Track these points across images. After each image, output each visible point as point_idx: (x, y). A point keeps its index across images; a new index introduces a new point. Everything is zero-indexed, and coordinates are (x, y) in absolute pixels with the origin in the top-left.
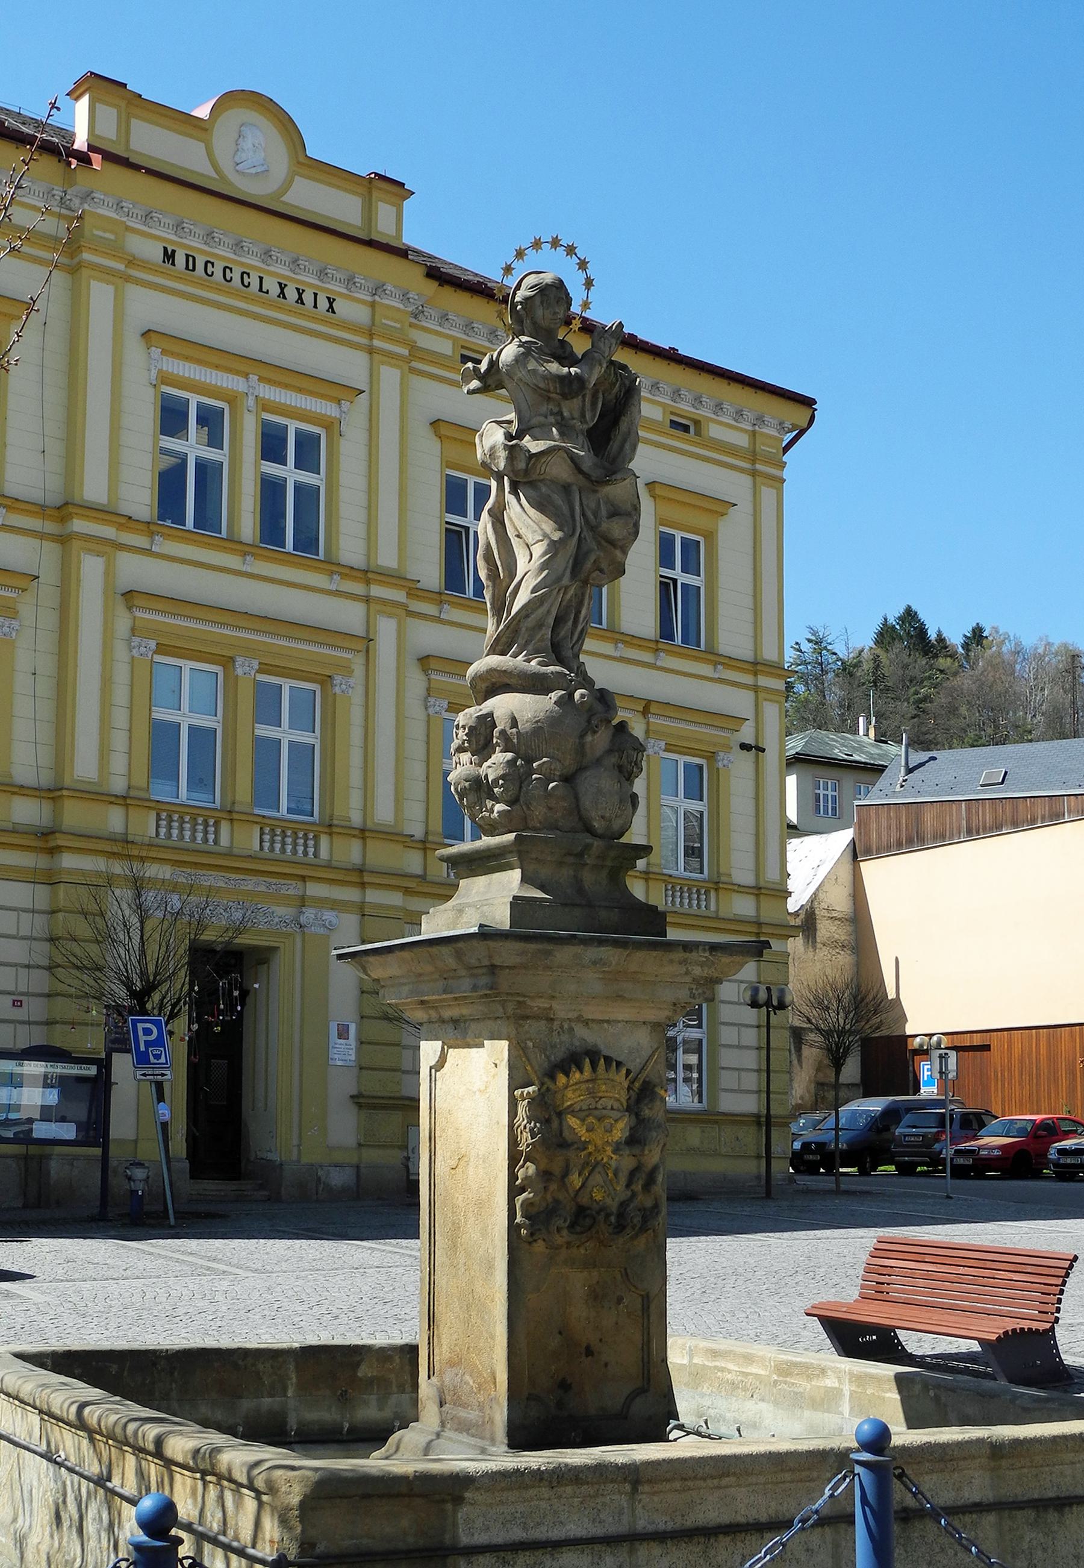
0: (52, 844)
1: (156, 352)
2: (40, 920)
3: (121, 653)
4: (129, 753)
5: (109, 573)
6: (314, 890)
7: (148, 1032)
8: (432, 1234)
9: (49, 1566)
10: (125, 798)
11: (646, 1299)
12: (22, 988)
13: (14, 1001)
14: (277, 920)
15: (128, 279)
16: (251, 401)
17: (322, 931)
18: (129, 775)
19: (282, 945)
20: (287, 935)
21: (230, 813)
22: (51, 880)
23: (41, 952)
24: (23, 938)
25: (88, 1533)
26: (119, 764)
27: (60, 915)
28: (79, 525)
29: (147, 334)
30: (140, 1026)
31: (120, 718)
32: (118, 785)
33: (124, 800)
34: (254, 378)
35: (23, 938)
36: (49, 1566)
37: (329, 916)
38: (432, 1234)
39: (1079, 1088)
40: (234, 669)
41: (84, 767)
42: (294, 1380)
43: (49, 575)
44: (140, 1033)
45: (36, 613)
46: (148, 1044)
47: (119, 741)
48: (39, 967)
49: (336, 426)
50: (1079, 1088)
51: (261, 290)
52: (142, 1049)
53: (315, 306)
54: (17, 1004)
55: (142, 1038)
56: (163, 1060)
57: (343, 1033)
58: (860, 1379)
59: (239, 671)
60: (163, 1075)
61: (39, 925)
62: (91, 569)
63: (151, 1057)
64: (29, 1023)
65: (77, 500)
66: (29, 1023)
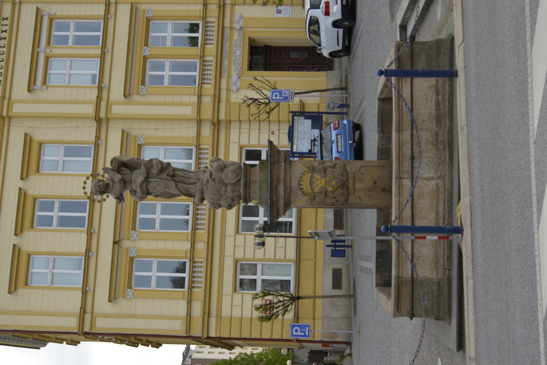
0: (217, 123)
1: (35, 87)
2: (243, 126)
4: (182, 95)
9: (350, 11)
12: (268, 131)
15: (10, 98)
17: (242, 20)
18: (190, 95)
19: (248, 36)
20: (244, 33)
21: (202, 57)
24: (250, 131)
26: (186, 99)
29: (29, 91)
31: (169, 99)
32: (194, 99)
33: (200, 97)
35: (250, 131)
36: (350, 11)
37: (237, 18)
39: (542, 339)
41: (189, 111)
42: (424, 59)
43: (126, 126)
45: (136, 129)
47: (177, 99)
49: (51, 17)
50: (542, 339)
51: (4, 47)
53: (2, 25)
57: (279, 12)
61: (245, 126)
62: (116, 110)
64: (279, 130)
65: (94, 115)
66: (279, 130)
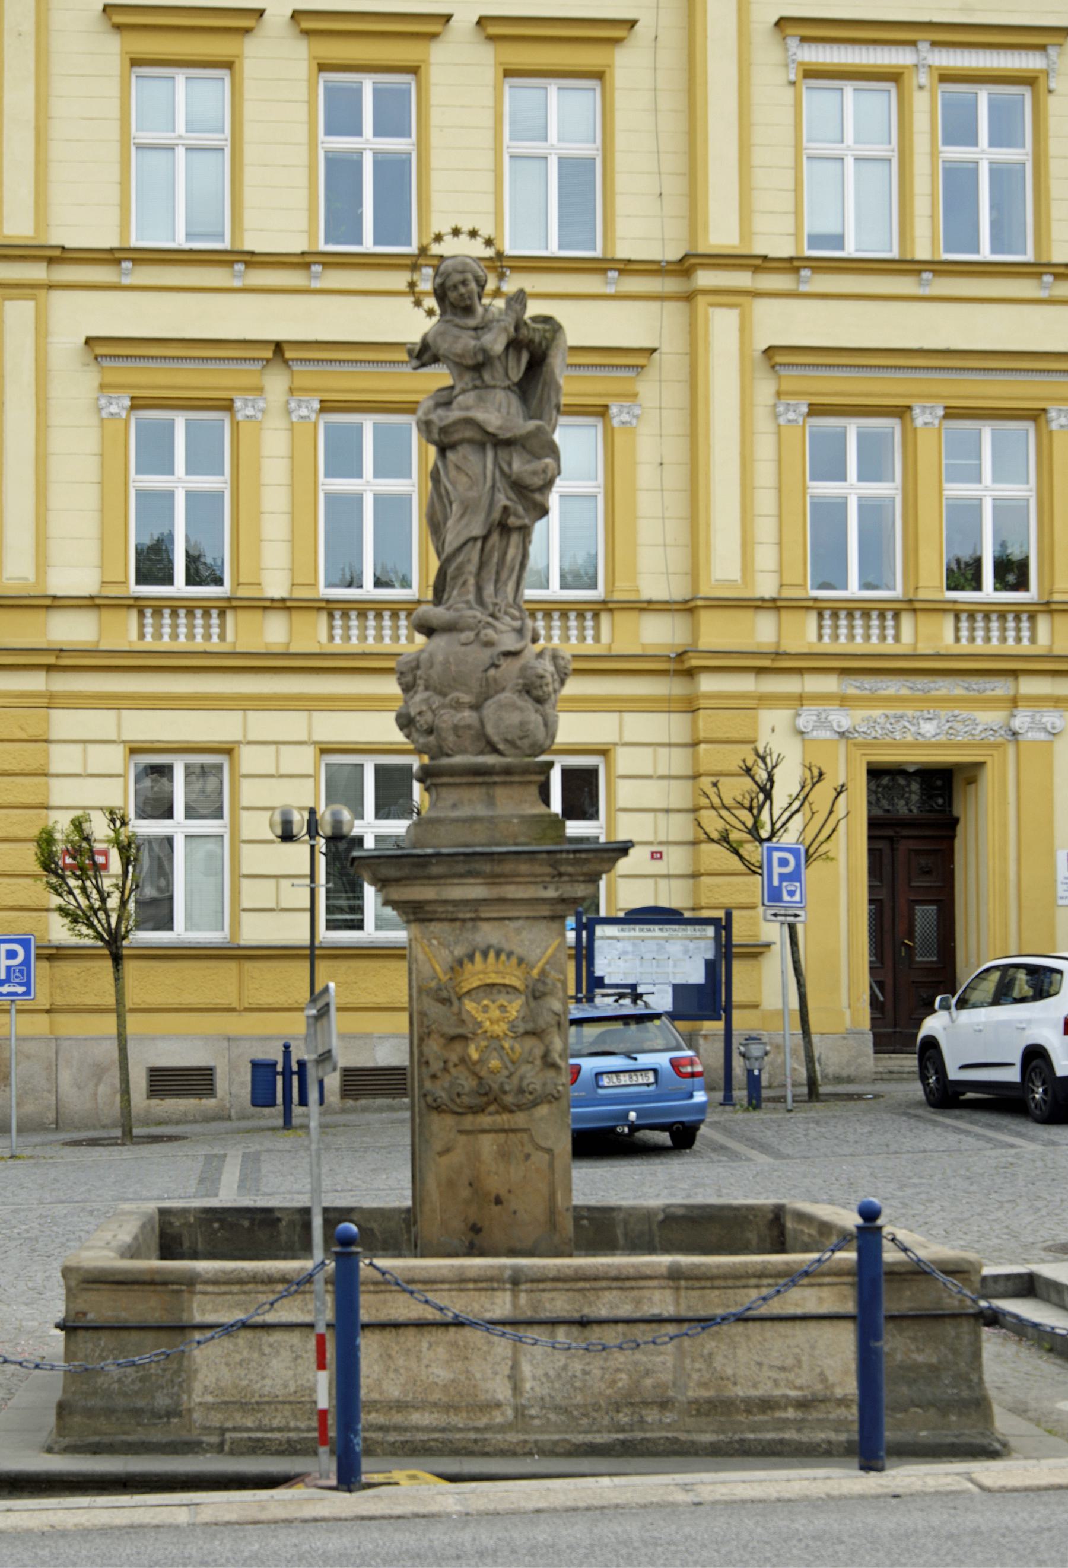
0: (686, 666)
3: (763, 424)
5: (745, 329)
6: (1029, 686)
7: (783, 862)
8: (911, 396)
10: (774, 600)
11: (590, 792)
12: (662, 838)
13: (653, 853)
14: (980, 728)
16: (923, 79)
17: (1042, 736)
18: (780, 571)
21: (912, 606)
22: (690, 706)
23: (679, 795)
25: (911, 1309)
26: (766, 557)
27: (702, 746)
28: (705, 278)
29: (782, 23)
30: (776, 855)
31: (765, 501)
32: (766, 588)
33: (774, 605)
34: (924, 47)
38: (911, 396)
40: (912, 420)
41: (724, 570)
44: (775, 863)
46: (783, 877)
47: (765, 529)
48: (679, 811)
52: (776, 883)
54: (656, 856)
55: (777, 870)
56: (797, 898)
58: (292, 1200)
59: (919, 422)
60: (796, 916)
63: (785, 894)
